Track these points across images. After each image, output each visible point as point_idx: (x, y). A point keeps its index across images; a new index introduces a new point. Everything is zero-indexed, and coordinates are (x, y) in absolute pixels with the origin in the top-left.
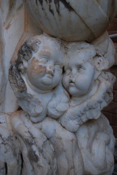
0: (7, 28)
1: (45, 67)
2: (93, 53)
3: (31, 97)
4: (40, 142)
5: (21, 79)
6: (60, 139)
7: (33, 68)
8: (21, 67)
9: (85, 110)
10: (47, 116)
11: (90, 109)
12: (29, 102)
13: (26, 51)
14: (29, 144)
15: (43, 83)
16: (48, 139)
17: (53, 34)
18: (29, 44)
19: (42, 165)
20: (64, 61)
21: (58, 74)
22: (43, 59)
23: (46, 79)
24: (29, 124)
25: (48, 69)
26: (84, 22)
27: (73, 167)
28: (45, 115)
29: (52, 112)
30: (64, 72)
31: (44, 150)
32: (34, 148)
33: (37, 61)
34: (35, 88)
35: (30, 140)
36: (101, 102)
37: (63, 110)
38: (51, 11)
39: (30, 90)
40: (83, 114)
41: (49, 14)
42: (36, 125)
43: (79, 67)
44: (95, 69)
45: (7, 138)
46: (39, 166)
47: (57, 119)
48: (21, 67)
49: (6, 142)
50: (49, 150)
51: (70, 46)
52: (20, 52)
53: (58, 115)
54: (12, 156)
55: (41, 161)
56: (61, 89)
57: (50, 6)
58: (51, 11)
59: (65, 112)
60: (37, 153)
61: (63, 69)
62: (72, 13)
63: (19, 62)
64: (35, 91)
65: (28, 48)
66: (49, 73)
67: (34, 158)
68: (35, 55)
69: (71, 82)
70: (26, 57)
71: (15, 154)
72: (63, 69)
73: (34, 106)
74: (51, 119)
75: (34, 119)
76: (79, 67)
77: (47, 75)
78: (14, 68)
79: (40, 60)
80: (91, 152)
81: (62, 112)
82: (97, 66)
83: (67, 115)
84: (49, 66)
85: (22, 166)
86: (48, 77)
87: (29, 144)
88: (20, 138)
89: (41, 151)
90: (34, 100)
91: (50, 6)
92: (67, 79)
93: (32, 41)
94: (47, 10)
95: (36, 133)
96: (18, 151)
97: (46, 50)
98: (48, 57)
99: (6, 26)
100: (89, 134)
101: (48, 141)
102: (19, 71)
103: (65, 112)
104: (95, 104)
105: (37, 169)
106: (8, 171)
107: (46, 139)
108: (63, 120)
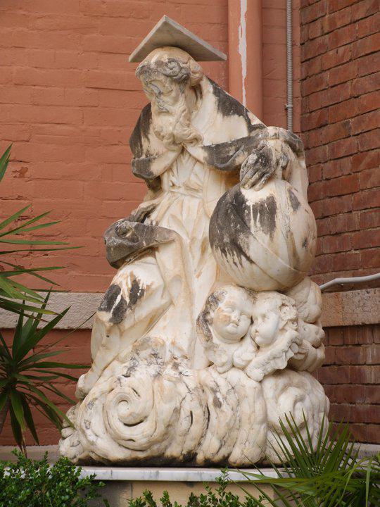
0: (198, 276)
1: (230, 317)
2: (280, 303)
3: (217, 346)
4: (224, 389)
5: (208, 328)
6: (244, 386)
7: (218, 318)
8: (208, 317)
9: (269, 359)
10: (233, 366)
11: (274, 358)
12: (215, 352)
13: (212, 301)
14: (214, 391)
15: (228, 332)
16: (233, 388)
17: (241, 284)
18: (216, 294)
19: (225, 410)
20: (249, 309)
21: (244, 323)
22: (229, 309)
23: (230, 328)
24: (215, 375)
25: (233, 318)
26: (265, 273)
27: (254, 412)
28: (231, 365)
29: (238, 361)
30: (252, 322)
31: (228, 397)
32: (219, 395)
33: (223, 311)
34: (221, 338)
35: (215, 387)
36: (286, 352)
37: (248, 359)
38: (235, 263)
39: (216, 340)
40: (268, 363)
41: (233, 266)
42: (222, 375)
43: (264, 316)
44: (280, 318)
45: (193, 388)
46: (222, 411)
47: (243, 369)
48: (208, 317)
49: (193, 392)
50: (232, 398)
51: (259, 296)
52: (208, 302)
53: (243, 364)
54: (198, 405)
55: (224, 407)
56: (248, 340)
57: (233, 259)
58: (235, 263)
59: (250, 361)
60: (221, 400)
61: (252, 319)
62: (254, 265)
63: (206, 313)
64: (221, 341)
65: (215, 298)
66: (234, 322)
67: (218, 404)
68: (221, 305)
69: (257, 332)
70: (213, 307)
71: (201, 405)
72: (252, 319)
73: (220, 355)
74: (237, 369)
75: (221, 370)
76: (264, 316)
77: (231, 324)
78: (201, 318)
79: (225, 310)
80: (277, 403)
81: (246, 361)
82: (283, 315)
83: (252, 364)
84: (234, 316)
85: (209, 419)
86: (233, 326)
87: (214, 391)
88: (49, 252)
89: (225, 398)
90: (219, 349)
91: (233, 259)
92: (254, 328)
93: (219, 292)
94: (231, 263)
95: (221, 382)
96: (204, 404)
97: (232, 301)
98: (233, 307)
99: (197, 274)
100: (277, 386)
101: (232, 390)
102: (206, 321)
103: (250, 361)
104: (280, 353)
105: (220, 415)
106: (194, 420)
107: (230, 388)
108: (248, 369)
